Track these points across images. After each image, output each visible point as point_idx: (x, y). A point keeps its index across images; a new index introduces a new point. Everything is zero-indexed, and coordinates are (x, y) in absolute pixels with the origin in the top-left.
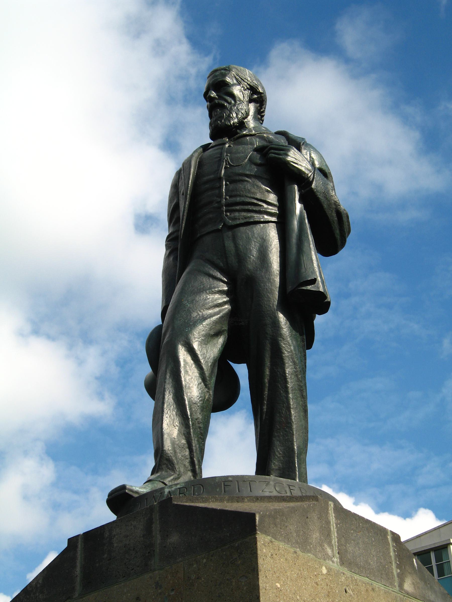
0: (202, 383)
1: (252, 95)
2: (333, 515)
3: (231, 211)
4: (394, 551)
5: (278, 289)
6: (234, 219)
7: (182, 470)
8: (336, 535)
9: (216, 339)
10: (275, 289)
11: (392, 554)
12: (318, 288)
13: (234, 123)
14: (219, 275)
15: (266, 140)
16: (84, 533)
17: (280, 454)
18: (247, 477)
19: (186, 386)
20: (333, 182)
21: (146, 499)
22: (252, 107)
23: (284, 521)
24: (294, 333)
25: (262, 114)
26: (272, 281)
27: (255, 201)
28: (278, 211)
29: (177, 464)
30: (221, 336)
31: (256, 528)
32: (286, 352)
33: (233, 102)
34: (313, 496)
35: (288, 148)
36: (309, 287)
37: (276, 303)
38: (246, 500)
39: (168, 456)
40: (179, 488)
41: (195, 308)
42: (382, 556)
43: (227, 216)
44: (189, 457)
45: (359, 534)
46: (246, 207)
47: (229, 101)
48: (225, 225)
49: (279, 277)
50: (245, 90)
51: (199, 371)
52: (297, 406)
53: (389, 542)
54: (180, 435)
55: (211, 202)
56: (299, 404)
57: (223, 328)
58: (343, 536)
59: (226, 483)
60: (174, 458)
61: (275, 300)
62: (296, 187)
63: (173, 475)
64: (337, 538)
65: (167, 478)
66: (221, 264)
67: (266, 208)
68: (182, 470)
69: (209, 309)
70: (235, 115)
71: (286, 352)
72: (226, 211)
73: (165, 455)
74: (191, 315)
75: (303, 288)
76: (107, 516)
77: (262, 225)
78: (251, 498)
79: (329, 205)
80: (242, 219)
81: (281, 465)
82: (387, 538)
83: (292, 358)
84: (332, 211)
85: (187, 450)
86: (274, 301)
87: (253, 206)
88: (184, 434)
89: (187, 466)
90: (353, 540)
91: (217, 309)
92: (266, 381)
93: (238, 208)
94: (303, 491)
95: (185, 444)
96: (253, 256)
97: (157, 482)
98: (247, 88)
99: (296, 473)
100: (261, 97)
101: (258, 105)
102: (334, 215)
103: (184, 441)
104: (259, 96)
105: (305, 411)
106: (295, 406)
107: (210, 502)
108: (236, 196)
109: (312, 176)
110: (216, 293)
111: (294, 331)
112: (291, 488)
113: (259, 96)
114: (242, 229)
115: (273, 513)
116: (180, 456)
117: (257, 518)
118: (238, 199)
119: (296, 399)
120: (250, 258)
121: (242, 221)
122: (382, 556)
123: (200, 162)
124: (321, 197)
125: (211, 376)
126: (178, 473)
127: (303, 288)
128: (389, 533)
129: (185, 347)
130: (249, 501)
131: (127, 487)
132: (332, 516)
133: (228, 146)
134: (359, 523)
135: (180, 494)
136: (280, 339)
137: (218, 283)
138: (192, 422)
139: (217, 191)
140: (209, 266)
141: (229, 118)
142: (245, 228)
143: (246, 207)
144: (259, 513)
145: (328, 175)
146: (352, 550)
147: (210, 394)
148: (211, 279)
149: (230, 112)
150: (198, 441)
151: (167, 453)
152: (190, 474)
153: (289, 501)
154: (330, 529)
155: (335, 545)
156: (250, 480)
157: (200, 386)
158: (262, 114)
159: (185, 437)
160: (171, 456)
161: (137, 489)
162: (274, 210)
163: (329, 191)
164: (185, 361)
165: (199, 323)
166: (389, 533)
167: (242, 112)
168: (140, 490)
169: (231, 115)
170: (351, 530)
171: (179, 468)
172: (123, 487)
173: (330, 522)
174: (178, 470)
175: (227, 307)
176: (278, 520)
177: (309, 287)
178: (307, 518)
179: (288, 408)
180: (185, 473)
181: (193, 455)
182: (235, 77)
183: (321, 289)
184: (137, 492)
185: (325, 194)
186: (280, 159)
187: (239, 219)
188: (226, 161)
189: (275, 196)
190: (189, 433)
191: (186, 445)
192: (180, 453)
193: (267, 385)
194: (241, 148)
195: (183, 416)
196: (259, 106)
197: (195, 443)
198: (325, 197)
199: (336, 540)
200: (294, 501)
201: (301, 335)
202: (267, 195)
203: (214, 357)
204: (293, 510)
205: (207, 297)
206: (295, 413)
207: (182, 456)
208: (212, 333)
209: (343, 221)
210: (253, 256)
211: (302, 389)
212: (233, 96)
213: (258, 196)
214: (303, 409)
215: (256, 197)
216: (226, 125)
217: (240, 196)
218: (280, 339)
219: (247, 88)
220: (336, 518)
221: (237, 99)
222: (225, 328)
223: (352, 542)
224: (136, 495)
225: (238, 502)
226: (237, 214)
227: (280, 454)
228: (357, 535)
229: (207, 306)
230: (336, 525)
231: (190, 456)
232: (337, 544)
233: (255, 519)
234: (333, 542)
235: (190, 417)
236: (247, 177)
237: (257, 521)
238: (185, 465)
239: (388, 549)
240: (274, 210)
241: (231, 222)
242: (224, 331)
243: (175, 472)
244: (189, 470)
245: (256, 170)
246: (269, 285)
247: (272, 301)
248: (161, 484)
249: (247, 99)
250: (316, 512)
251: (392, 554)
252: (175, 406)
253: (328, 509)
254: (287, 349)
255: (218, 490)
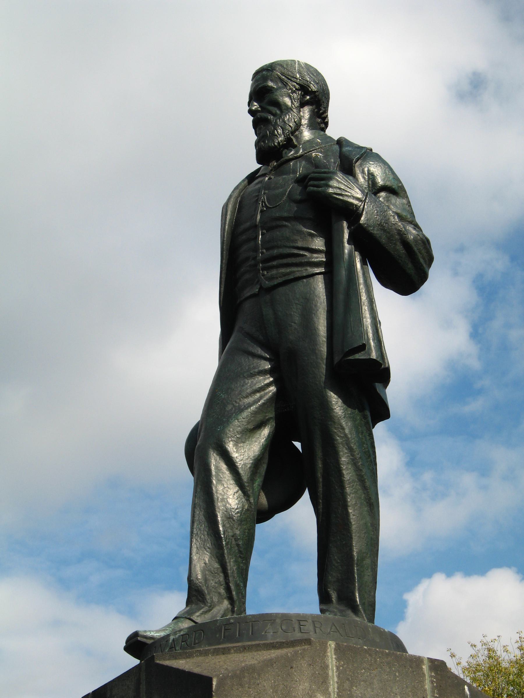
0: (240, 492)
1: (303, 96)
2: (334, 657)
3: (268, 269)
4: (432, 682)
5: (325, 361)
6: (271, 278)
7: (215, 599)
8: (336, 679)
9: (259, 432)
10: (321, 362)
11: (428, 686)
12: (370, 354)
13: (279, 143)
14: (259, 351)
15: (312, 163)
16: (93, 692)
17: (337, 563)
18: (250, 617)
19: (218, 499)
20: (407, 197)
21: (155, 647)
22: (306, 113)
23: (256, 678)
24: (350, 411)
25: (323, 116)
26: (317, 352)
27: (296, 251)
28: (326, 258)
29: (209, 594)
30: (265, 426)
31: (212, 694)
32: (338, 438)
33: (278, 112)
34: (306, 640)
35: (329, 175)
36: (358, 356)
37: (323, 378)
38: (232, 651)
39: (197, 587)
40: (182, 635)
41: (230, 399)
42: (410, 691)
43: (263, 275)
44: (223, 583)
45: (375, 672)
46: (285, 261)
47: (274, 112)
48: (261, 288)
49: (326, 345)
50: (293, 92)
51: (235, 477)
52: (356, 501)
53: (424, 674)
54: (213, 559)
55: (247, 259)
56: (360, 498)
57: (266, 416)
58: (348, 679)
59: (227, 627)
60: (204, 588)
61: (322, 376)
62: (345, 224)
63: (203, 607)
64: (337, 683)
65: (196, 612)
66: (261, 338)
67: (309, 258)
68: (215, 599)
69: (247, 397)
70: (280, 131)
71: (338, 438)
72: (263, 269)
73: (193, 585)
74: (225, 408)
75: (351, 358)
76: (133, 662)
77: (305, 280)
78: (238, 648)
79: (390, 238)
80: (280, 277)
81: (339, 575)
82: (422, 668)
83: (347, 444)
84: (395, 244)
85: (222, 575)
86: (321, 377)
87: (295, 258)
88: (217, 557)
89: (222, 594)
90: (363, 681)
91: (258, 395)
92: (319, 475)
93: (275, 263)
94: (316, 626)
95: (217, 568)
96: (295, 323)
97: (182, 619)
98: (296, 89)
99: (354, 585)
100: (316, 96)
101: (314, 107)
102: (400, 247)
103: (217, 565)
104: (313, 96)
105: (370, 505)
106: (354, 503)
107: (194, 657)
108: (273, 248)
109: (362, 207)
110: (255, 375)
111: (349, 409)
112: (302, 623)
113: (313, 96)
114: (281, 290)
115: (238, 672)
116: (212, 583)
117: (214, 683)
118: (275, 252)
119: (356, 493)
120: (291, 326)
121: (280, 280)
122: (410, 691)
123: (241, 202)
124: (376, 232)
125: (252, 479)
126: (209, 604)
127: (351, 358)
128: (426, 662)
129: (217, 450)
130: (236, 652)
131: (140, 633)
132: (332, 658)
133: (269, 179)
134: (375, 658)
135: (182, 642)
136: (330, 423)
137: (259, 361)
138: (225, 541)
139: (252, 244)
140: (249, 341)
141: (273, 135)
142: (284, 288)
143: (285, 261)
144: (218, 676)
145: (399, 191)
146: (361, 693)
147: (250, 502)
148: (250, 358)
149: (274, 127)
150: (236, 561)
151: (195, 583)
152: (226, 604)
153: (278, 648)
154: (328, 674)
155: (334, 692)
156: (253, 620)
157: (236, 495)
158: (323, 116)
159: (218, 560)
160: (200, 586)
161: (152, 634)
162: (322, 258)
163: (389, 219)
164: (217, 468)
165: (234, 417)
166: (426, 662)
167: (291, 124)
168: (156, 635)
169: (276, 133)
170: (362, 670)
171: (212, 598)
172: (136, 634)
173: (327, 666)
174: (209, 601)
175: (273, 389)
176: (246, 679)
177: (358, 356)
178: (292, 668)
179: (345, 506)
180: (220, 602)
181: (229, 580)
182: (280, 78)
183: (374, 355)
184: (152, 638)
185: (382, 225)
186: (319, 192)
187: (277, 278)
188: (262, 202)
189: (321, 239)
190: (222, 555)
191: (220, 570)
192: (213, 580)
193: (321, 480)
194: (280, 180)
195: (215, 536)
196: (316, 108)
197: (231, 565)
198: (382, 229)
199: (336, 685)
200: (285, 647)
201: (361, 410)
202: (310, 239)
203: (254, 457)
204: (270, 663)
205: (244, 382)
206: (354, 511)
207: (216, 583)
208: (250, 426)
209: (414, 251)
210: (295, 323)
211: (363, 479)
212: (277, 104)
213: (300, 244)
214: (367, 503)
215: (297, 245)
216: (269, 146)
217: (278, 247)
218: (330, 423)
219: (296, 89)
220: (338, 659)
221: (283, 107)
222: (271, 414)
223: (362, 683)
224: (149, 642)
225: (224, 654)
226: (274, 272)
227: (337, 563)
228: (370, 673)
229: (244, 394)
230: (338, 668)
231: (225, 581)
232: (336, 690)
233: (211, 684)
234: (331, 689)
235: (222, 536)
236: (286, 221)
237: (214, 686)
238: (219, 593)
239: (422, 682)
240: (322, 258)
241: (267, 284)
242: (271, 418)
243: (205, 604)
244: (225, 598)
245: (296, 209)
246: (314, 358)
247: (319, 377)
248: (188, 621)
249: (297, 104)
250: (306, 659)
251: (428, 686)
252: (206, 525)
253: (325, 651)
254: (339, 434)
255: (218, 636)
